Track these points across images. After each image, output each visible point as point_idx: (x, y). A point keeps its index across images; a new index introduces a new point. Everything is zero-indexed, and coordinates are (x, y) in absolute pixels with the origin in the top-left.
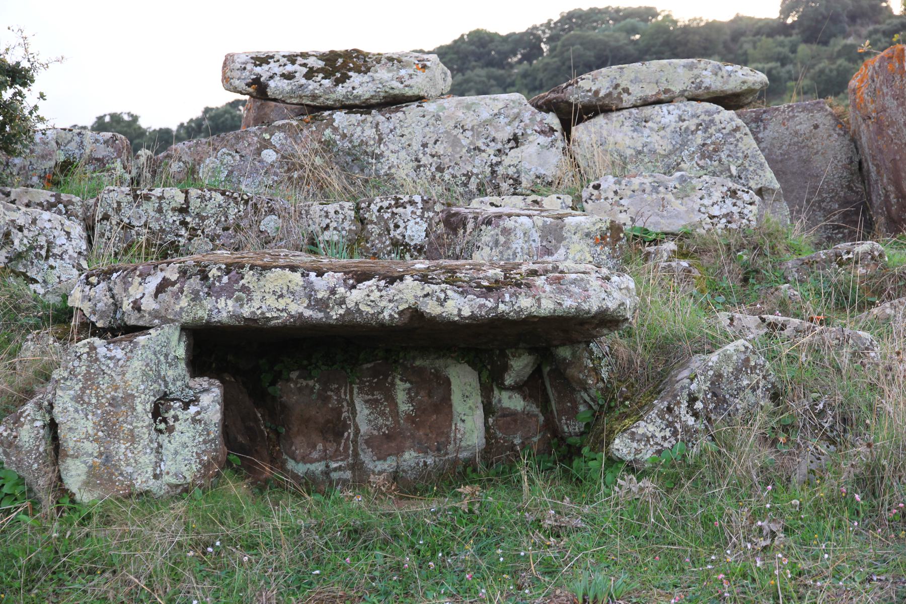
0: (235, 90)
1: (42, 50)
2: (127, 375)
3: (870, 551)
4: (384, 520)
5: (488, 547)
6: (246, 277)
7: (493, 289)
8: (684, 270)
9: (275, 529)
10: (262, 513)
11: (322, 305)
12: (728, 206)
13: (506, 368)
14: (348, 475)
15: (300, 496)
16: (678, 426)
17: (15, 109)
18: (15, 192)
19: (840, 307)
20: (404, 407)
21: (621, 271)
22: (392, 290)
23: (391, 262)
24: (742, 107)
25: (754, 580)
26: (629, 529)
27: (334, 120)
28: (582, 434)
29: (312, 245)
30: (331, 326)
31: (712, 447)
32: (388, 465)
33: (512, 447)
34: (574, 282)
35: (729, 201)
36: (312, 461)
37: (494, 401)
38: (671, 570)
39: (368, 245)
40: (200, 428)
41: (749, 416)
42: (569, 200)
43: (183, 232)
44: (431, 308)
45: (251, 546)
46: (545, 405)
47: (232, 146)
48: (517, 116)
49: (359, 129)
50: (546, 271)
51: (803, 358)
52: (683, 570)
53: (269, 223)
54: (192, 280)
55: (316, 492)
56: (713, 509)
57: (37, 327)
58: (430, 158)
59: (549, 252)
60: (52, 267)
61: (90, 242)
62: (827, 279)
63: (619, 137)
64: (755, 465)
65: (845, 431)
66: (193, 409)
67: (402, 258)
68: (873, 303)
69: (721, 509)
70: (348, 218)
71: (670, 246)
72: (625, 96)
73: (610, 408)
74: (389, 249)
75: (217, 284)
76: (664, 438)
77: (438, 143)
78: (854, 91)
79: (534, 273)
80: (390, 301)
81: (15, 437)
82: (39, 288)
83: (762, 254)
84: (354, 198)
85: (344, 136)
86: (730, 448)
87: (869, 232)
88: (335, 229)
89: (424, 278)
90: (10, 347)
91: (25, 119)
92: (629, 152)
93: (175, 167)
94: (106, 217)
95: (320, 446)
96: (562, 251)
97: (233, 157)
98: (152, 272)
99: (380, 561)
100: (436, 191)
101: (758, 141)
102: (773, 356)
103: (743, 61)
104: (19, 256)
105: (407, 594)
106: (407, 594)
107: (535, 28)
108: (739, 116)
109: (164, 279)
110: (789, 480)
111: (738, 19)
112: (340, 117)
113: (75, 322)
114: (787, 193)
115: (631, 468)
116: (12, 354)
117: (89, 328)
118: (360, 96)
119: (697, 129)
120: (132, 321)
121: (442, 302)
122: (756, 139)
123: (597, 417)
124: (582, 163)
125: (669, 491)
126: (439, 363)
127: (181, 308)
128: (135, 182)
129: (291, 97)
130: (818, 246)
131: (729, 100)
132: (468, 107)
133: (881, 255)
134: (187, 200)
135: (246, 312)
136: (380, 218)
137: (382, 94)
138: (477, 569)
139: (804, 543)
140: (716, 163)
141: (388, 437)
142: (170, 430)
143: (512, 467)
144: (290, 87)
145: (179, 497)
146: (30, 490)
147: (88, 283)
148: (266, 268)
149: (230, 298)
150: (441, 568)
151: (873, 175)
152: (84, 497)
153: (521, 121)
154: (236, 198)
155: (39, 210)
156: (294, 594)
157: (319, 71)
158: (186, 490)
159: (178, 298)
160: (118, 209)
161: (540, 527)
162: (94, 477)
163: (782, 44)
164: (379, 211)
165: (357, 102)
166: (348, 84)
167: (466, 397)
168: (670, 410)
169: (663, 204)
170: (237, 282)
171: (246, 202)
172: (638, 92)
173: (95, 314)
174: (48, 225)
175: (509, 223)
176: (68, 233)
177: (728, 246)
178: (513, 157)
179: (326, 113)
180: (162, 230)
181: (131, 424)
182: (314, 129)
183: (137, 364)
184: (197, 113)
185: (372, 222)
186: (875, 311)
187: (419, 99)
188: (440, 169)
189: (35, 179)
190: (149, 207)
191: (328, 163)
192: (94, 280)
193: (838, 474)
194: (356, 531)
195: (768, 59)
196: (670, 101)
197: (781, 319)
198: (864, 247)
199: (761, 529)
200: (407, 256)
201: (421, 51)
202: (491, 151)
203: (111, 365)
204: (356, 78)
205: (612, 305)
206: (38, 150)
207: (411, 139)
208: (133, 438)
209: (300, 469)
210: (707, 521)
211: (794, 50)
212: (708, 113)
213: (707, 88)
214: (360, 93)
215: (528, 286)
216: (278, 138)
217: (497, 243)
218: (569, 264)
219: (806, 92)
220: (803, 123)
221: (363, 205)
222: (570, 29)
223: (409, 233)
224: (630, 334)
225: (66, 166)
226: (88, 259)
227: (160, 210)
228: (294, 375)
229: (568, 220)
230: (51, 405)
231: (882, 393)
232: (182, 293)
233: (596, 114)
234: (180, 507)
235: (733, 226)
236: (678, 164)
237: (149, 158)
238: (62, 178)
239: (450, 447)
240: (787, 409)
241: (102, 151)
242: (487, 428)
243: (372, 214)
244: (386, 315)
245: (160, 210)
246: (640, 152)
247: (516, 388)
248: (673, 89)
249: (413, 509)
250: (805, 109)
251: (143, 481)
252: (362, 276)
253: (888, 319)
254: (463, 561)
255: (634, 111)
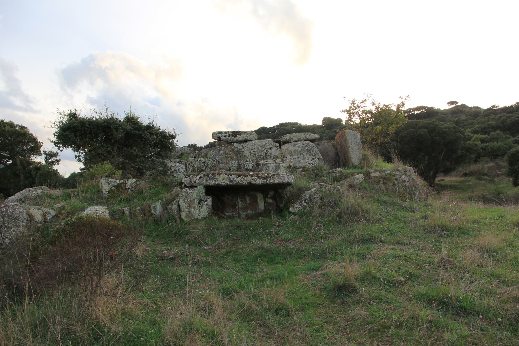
0: (215, 139)
1: (177, 132)
3: (339, 229)
4: (244, 224)
5: (265, 229)
7: (266, 178)
8: (304, 174)
9: (222, 226)
10: (220, 223)
11: (232, 181)
12: (312, 161)
13: (268, 194)
14: (237, 215)
15: (227, 220)
16: (303, 205)
17: (172, 143)
18: (172, 159)
19: (334, 181)
20: (248, 202)
21: (291, 174)
22: (245, 178)
23: (245, 173)
24: (315, 142)
25: (317, 235)
26: (293, 226)
28: (284, 207)
29: (230, 170)
30: (233, 186)
31: (309, 209)
32: (245, 213)
33: (270, 210)
34: (282, 177)
35: (312, 161)
36: (230, 213)
37: (266, 201)
38: (301, 234)
40: (208, 206)
41: (317, 202)
42: (281, 160)
43: (204, 167)
44: (253, 182)
45: (218, 229)
46: (276, 201)
48: (270, 144)
50: (276, 175)
51: (327, 191)
52: (303, 234)
53: (221, 165)
55: (231, 219)
56: (309, 221)
57: (176, 186)
59: (277, 171)
60: (179, 174)
61: (186, 169)
62: (331, 176)
63: (291, 148)
64: (317, 213)
65: (335, 206)
66: (206, 202)
67: (248, 172)
68: (340, 181)
69: (311, 221)
71: (301, 169)
72: (292, 140)
73: (289, 202)
76: (300, 208)
78: (336, 139)
79: (274, 175)
82: (176, 178)
83: (319, 171)
84: (238, 160)
85: (236, 148)
86: (313, 210)
87: (339, 167)
89: (252, 176)
90: (171, 190)
91: (174, 145)
92: (293, 151)
93: (203, 154)
94: (189, 164)
95: (231, 210)
96: (280, 170)
99: (244, 232)
100: (254, 159)
101: (318, 149)
102: (321, 191)
103: (315, 133)
104: (173, 172)
105: (249, 239)
106: (249, 239)
107: (274, 126)
108: (314, 144)
110: (324, 215)
111: (314, 125)
112: (235, 144)
113: (183, 185)
114: (324, 159)
115: (293, 214)
116: (171, 191)
117: (186, 186)
120: (194, 185)
121: (255, 181)
122: (318, 148)
123: (286, 203)
124: (283, 153)
125: (301, 218)
126: (112, 223)
128: (195, 157)
130: (330, 169)
131: (312, 141)
132: (261, 142)
133: (342, 171)
134: (205, 161)
135: (216, 183)
136: (243, 164)
138: (262, 234)
139: (327, 228)
141: (245, 208)
142: (202, 206)
143: (270, 214)
145: (204, 220)
146: (175, 218)
147: (186, 177)
148: (220, 174)
150: (256, 233)
151: (340, 156)
152: (185, 219)
155: (176, 163)
156: (226, 239)
157: (231, 135)
158: (205, 218)
159: (203, 180)
160: (192, 163)
161: (275, 226)
162: (187, 216)
163: (322, 130)
166: (237, 138)
167: (260, 200)
168: (301, 202)
169: (299, 161)
171: (217, 161)
172: (294, 139)
174: (178, 166)
175: (269, 165)
176: (182, 168)
177: (312, 169)
178: (270, 152)
180: (200, 167)
183: (195, 193)
184: (208, 144)
186: (341, 182)
187: (251, 140)
188: (255, 154)
189: (176, 157)
190: (198, 162)
191: (233, 153)
192: (187, 177)
193: (334, 214)
194: (239, 226)
195: (320, 133)
196: (301, 141)
197: (323, 184)
198: (338, 169)
199: (319, 225)
200: (249, 172)
201: (252, 131)
202: (265, 151)
204: (238, 136)
205: (289, 181)
206: (176, 151)
208: (194, 208)
209: (228, 214)
210: (308, 224)
211: (325, 131)
212: (308, 143)
215: (273, 177)
216: (223, 148)
217: (266, 169)
218: (281, 173)
219: (327, 139)
220: (326, 145)
222: (281, 127)
223: (249, 167)
224: (293, 187)
225: (182, 154)
226: (186, 172)
227: (200, 163)
228: (226, 195)
229: (281, 164)
230: (179, 202)
231: (342, 198)
233: (286, 143)
234: (204, 222)
235: (313, 165)
237: (198, 153)
238: (181, 157)
239: (257, 210)
240: (324, 201)
241: (189, 151)
242: (265, 206)
243: (242, 163)
244: (244, 183)
245: (200, 163)
246: (295, 151)
247: (271, 198)
249: (250, 222)
250: (327, 143)
251: (197, 216)
252: (240, 176)
253: (343, 184)
254: (260, 232)
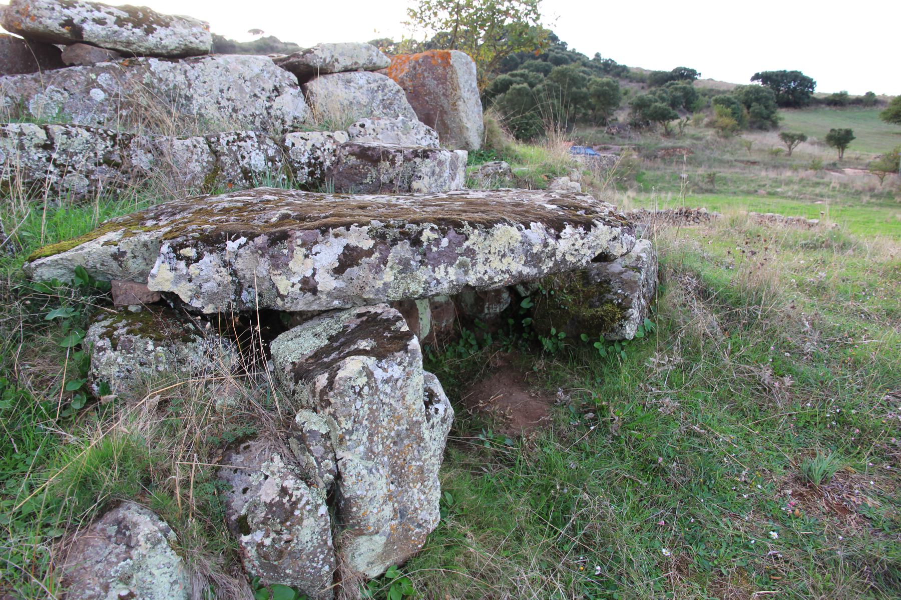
2: (408, 398)
6: (472, 237)
11: (534, 259)
27: (150, 66)
39: (224, 174)
47: (60, 84)
49: (171, 75)
54: (398, 247)
58: (226, 101)
70: (205, 151)
74: (241, 176)
75: (435, 249)
77: (230, 90)
80: (589, 248)
81: (288, 542)
85: (160, 80)
88: (197, 160)
92: (346, 103)
97: (62, 94)
98: (320, 238)
109: (347, 247)
112: (153, 62)
118: (167, 46)
119: (378, 90)
127: (385, 284)
129: (106, 42)
135: (472, 280)
136: (230, 150)
137: (183, 47)
140: (392, 112)
144: (105, 32)
149: (452, 266)
153: (276, 77)
154: (102, 134)
164: (228, 144)
165: (164, 51)
170: (460, 244)
173: (198, 298)
178: (278, 103)
179: (141, 59)
181: (420, 460)
182: (135, 72)
185: (224, 154)
188: (235, 110)
203: (388, 390)
204: (161, 32)
207: (211, 86)
213: (374, 64)
214: (167, 44)
217: (433, 173)
221: (213, 140)
227: (21, 147)
232: (385, 265)
236: (372, 112)
243: (223, 147)
248: (359, 62)
255: (341, 75)
